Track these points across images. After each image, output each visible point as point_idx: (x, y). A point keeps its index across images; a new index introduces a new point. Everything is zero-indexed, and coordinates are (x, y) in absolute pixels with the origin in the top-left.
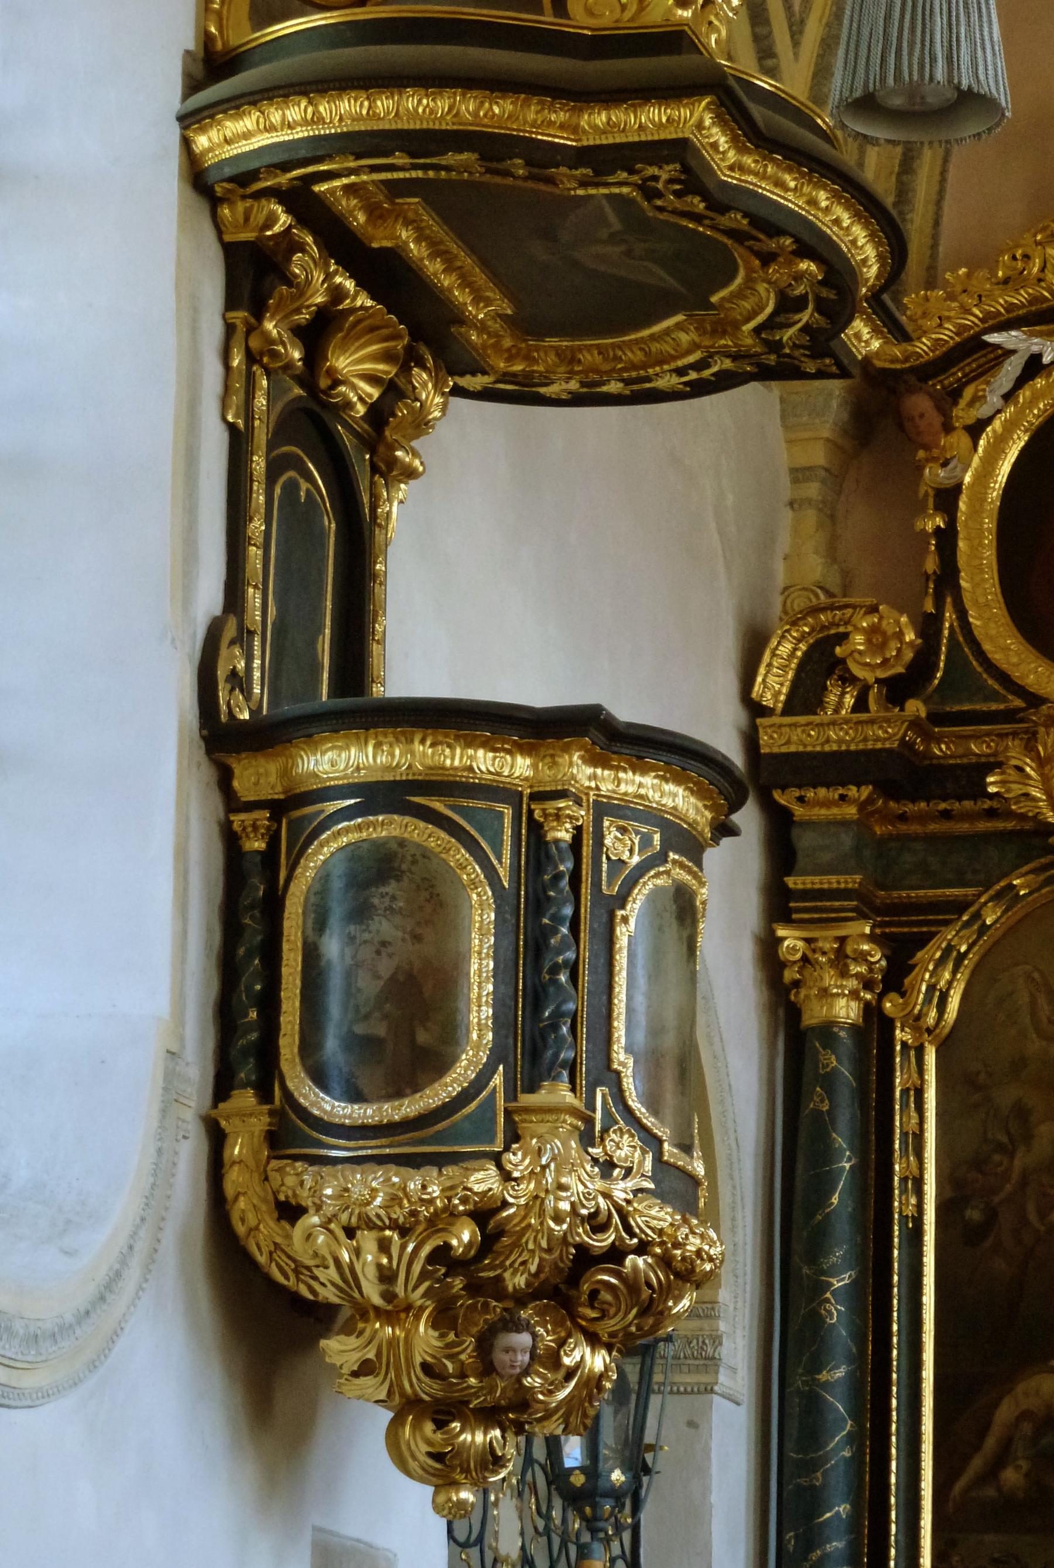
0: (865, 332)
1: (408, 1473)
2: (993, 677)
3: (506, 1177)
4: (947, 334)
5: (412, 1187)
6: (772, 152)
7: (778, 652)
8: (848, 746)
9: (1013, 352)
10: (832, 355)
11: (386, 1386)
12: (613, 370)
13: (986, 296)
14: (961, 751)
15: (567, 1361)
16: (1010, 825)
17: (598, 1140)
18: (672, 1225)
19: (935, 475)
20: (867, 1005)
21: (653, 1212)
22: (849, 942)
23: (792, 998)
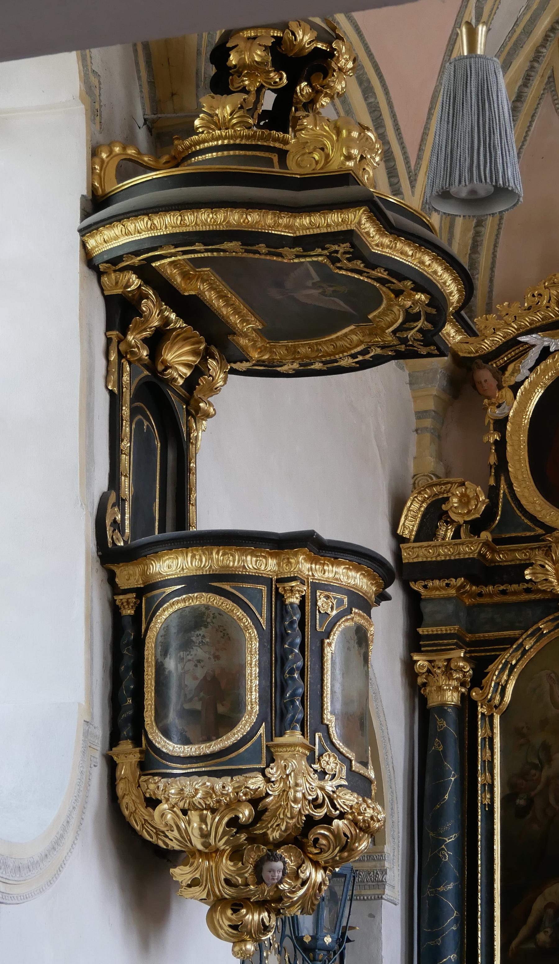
0: (452, 332)
1: (219, 936)
2: (527, 518)
3: (268, 780)
4: (499, 338)
5: (217, 787)
6: (399, 236)
7: (411, 508)
8: (450, 557)
9: (534, 346)
10: (435, 344)
11: (206, 891)
12: (317, 357)
13: (518, 316)
14: (510, 558)
15: (302, 875)
16: (538, 596)
17: (317, 760)
18: (357, 803)
19: (494, 413)
20: (463, 694)
21: (347, 797)
22: (452, 661)
23: (422, 692)
